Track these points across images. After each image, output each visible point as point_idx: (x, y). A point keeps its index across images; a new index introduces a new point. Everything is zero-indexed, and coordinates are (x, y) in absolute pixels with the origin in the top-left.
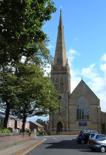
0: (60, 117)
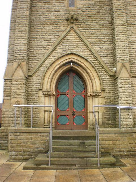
0: (72, 38)
